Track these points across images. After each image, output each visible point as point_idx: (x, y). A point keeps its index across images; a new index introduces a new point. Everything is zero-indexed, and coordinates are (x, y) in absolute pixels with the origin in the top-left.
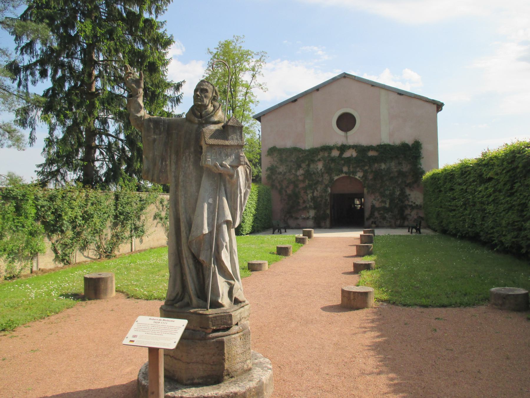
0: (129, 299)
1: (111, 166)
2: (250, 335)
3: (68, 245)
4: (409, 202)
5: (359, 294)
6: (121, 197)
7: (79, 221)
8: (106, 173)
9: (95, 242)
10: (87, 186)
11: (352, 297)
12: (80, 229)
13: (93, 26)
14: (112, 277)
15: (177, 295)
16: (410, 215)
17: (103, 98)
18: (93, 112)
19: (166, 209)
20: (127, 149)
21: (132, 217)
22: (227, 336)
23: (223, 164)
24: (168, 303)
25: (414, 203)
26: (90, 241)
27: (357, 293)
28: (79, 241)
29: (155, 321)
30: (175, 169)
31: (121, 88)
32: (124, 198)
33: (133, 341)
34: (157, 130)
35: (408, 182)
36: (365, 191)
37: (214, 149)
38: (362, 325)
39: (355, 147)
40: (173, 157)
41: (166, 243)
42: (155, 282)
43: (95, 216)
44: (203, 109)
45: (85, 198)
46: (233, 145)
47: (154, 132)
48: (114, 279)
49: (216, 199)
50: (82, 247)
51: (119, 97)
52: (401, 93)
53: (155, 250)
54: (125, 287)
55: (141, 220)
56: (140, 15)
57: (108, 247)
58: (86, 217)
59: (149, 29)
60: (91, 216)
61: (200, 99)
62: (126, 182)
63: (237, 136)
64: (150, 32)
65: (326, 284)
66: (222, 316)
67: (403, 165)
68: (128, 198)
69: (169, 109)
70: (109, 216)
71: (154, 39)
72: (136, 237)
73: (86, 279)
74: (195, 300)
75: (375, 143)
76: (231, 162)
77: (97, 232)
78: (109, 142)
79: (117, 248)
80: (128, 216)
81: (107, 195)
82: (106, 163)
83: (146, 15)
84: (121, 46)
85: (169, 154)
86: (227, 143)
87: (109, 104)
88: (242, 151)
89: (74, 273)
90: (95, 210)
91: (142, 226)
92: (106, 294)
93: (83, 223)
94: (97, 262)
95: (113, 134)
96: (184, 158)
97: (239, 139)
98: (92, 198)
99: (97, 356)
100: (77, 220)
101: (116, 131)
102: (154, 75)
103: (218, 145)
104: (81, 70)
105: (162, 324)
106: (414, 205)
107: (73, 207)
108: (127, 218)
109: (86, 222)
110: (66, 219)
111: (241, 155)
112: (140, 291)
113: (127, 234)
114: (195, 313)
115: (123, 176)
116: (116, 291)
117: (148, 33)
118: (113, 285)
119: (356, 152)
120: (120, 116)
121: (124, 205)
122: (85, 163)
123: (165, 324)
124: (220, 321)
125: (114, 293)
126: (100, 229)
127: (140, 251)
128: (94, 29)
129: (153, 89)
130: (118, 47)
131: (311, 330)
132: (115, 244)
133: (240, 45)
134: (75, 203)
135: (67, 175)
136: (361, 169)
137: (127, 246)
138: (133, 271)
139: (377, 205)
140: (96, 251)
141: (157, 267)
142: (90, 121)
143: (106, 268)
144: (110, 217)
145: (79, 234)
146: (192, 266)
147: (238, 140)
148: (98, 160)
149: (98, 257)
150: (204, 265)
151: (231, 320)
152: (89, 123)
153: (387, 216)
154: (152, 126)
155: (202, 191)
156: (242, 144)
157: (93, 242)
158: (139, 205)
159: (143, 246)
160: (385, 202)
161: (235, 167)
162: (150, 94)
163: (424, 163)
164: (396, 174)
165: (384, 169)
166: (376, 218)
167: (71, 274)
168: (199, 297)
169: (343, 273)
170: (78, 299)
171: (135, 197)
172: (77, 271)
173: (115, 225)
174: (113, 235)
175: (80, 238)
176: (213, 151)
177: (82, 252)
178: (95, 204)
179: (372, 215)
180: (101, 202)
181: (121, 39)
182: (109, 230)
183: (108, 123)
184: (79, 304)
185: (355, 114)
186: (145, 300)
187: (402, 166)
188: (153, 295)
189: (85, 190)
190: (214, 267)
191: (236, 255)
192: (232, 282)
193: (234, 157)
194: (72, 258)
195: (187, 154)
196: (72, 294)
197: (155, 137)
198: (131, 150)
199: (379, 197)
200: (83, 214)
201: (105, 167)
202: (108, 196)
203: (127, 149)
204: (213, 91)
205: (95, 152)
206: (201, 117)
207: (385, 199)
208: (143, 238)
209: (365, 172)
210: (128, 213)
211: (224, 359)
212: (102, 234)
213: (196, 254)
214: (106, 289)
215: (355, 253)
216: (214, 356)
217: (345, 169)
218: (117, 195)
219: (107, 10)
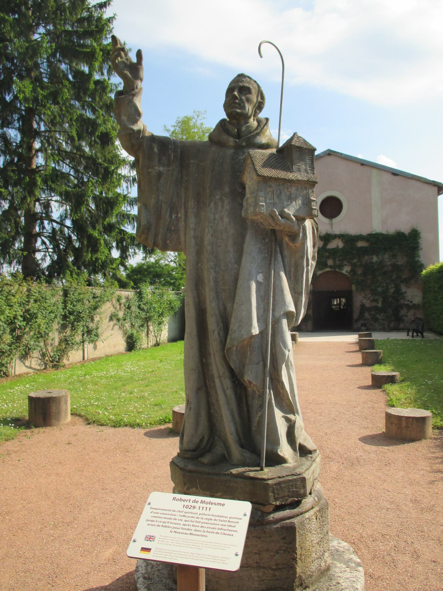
0: (89, 426)
1: (56, 257)
2: (327, 509)
3: (6, 352)
4: (405, 300)
5: (414, 421)
6: (71, 293)
7: (20, 322)
8: (49, 266)
9: (39, 349)
10: (29, 278)
11: (404, 424)
12: (20, 332)
13: (33, 87)
14: (66, 396)
15: (202, 440)
16: (407, 316)
17: (46, 175)
18: (34, 191)
19: (124, 308)
20: (74, 237)
21: (84, 317)
22: (298, 515)
23: (285, 211)
24: (187, 455)
25: (411, 302)
26: (33, 348)
27: (411, 419)
28: (19, 347)
29: (186, 503)
30: (195, 225)
31: (67, 164)
32: (75, 294)
33: (148, 550)
34: (164, 158)
35: (403, 277)
36: (354, 287)
37: (270, 186)
38: (435, 467)
39: (342, 237)
40: (191, 203)
41: (124, 350)
42: (121, 402)
43: (39, 316)
44: (243, 122)
45: (27, 293)
46: (301, 181)
47: (159, 161)
48: (69, 399)
49: (270, 274)
50: (22, 354)
51: (65, 176)
52: (395, 173)
53: (113, 358)
54: (82, 408)
55: (95, 321)
56: (90, 75)
57: (55, 355)
58: (28, 318)
59: (100, 93)
60: (34, 316)
61: (240, 104)
62: (75, 276)
63: (306, 166)
64: (102, 96)
65: (345, 403)
66: (290, 481)
67: (399, 257)
68: (79, 294)
69: (123, 190)
70: (56, 317)
71: (107, 104)
72: (89, 343)
73: (31, 399)
74: (236, 451)
75: (365, 232)
76: (297, 211)
77: (41, 336)
78: (54, 229)
79: (66, 355)
80: (79, 316)
81: (54, 290)
82: (49, 255)
83: (97, 77)
84: (68, 112)
85: (183, 201)
86: (291, 176)
87: (53, 182)
88: (313, 192)
89: (14, 388)
90: (39, 308)
91: (96, 329)
92: (58, 419)
93: (25, 325)
94: (42, 374)
95: (58, 220)
96: (212, 205)
97: (309, 171)
98: (35, 293)
99: (55, 526)
100: (16, 321)
101: (61, 216)
102: (107, 149)
103: (277, 179)
104: (18, 142)
105: (201, 511)
106: (410, 304)
107: (12, 304)
108: (78, 319)
109: (27, 324)
110: (3, 320)
111: (312, 198)
112: (102, 414)
113: (78, 338)
114: (241, 476)
115: (70, 269)
116: (72, 414)
117: (100, 98)
118: (68, 407)
119: (343, 243)
120: (66, 197)
121: (75, 303)
122: (25, 253)
123: (207, 512)
124: (287, 490)
125: (69, 418)
126: (45, 332)
127: (94, 360)
128: (34, 90)
129: (106, 165)
130: (63, 113)
131: (365, 475)
132: (63, 351)
133: (201, 122)
134: (14, 300)
135: (3, 268)
136: (349, 262)
137: (78, 353)
138: (90, 386)
139: (368, 304)
140: (40, 359)
141: (121, 381)
142: (31, 201)
143: (54, 382)
144: (58, 317)
145: (18, 338)
146: (230, 392)
147: (307, 173)
148: (39, 251)
149: (43, 367)
150: (250, 390)
151: (304, 487)
152: (29, 205)
153: (379, 317)
154: (156, 150)
155: (246, 260)
156: (314, 180)
157: (37, 349)
158: (93, 302)
159: (98, 353)
160: (377, 301)
161: (301, 220)
162: (103, 170)
163: (423, 256)
164: (390, 268)
165: (376, 261)
166: (366, 320)
167: (9, 390)
168: (242, 446)
169: (359, 388)
170: (20, 426)
171: (87, 293)
172: (17, 386)
173: (64, 327)
174: (61, 340)
175: (20, 343)
176: (269, 189)
177: (22, 362)
178: (39, 300)
179: (362, 313)
180: (46, 299)
181: (67, 104)
182: (57, 334)
183: (51, 207)
184: (23, 434)
185: (342, 198)
186: (112, 426)
187: (397, 258)
188: (122, 420)
189: (26, 283)
190: (270, 394)
191: (293, 371)
192: (291, 416)
193: (300, 202)
194: (11, 369)
195: (218, 197)
196: (12, 419)
197: (161, 169)
198: (79, 240)
199: (370, 296)
200: (24, 313)
201: (48, 259)
202: (55, 291)
203: (74, 237)
204: (258, 93)
205: (36, 241)
206: (238, 136)
207: (376, 297)
208: (97, 343)
209: (354, 266)
210: (79, 312)
211: (295, 559)
212: (47, 339)
213: (237, 371)
214: (59, 413)
215: (360, 361)
216: (277, 553)
217: (330, 262)
218: (66, 290)
219: (49, 70)
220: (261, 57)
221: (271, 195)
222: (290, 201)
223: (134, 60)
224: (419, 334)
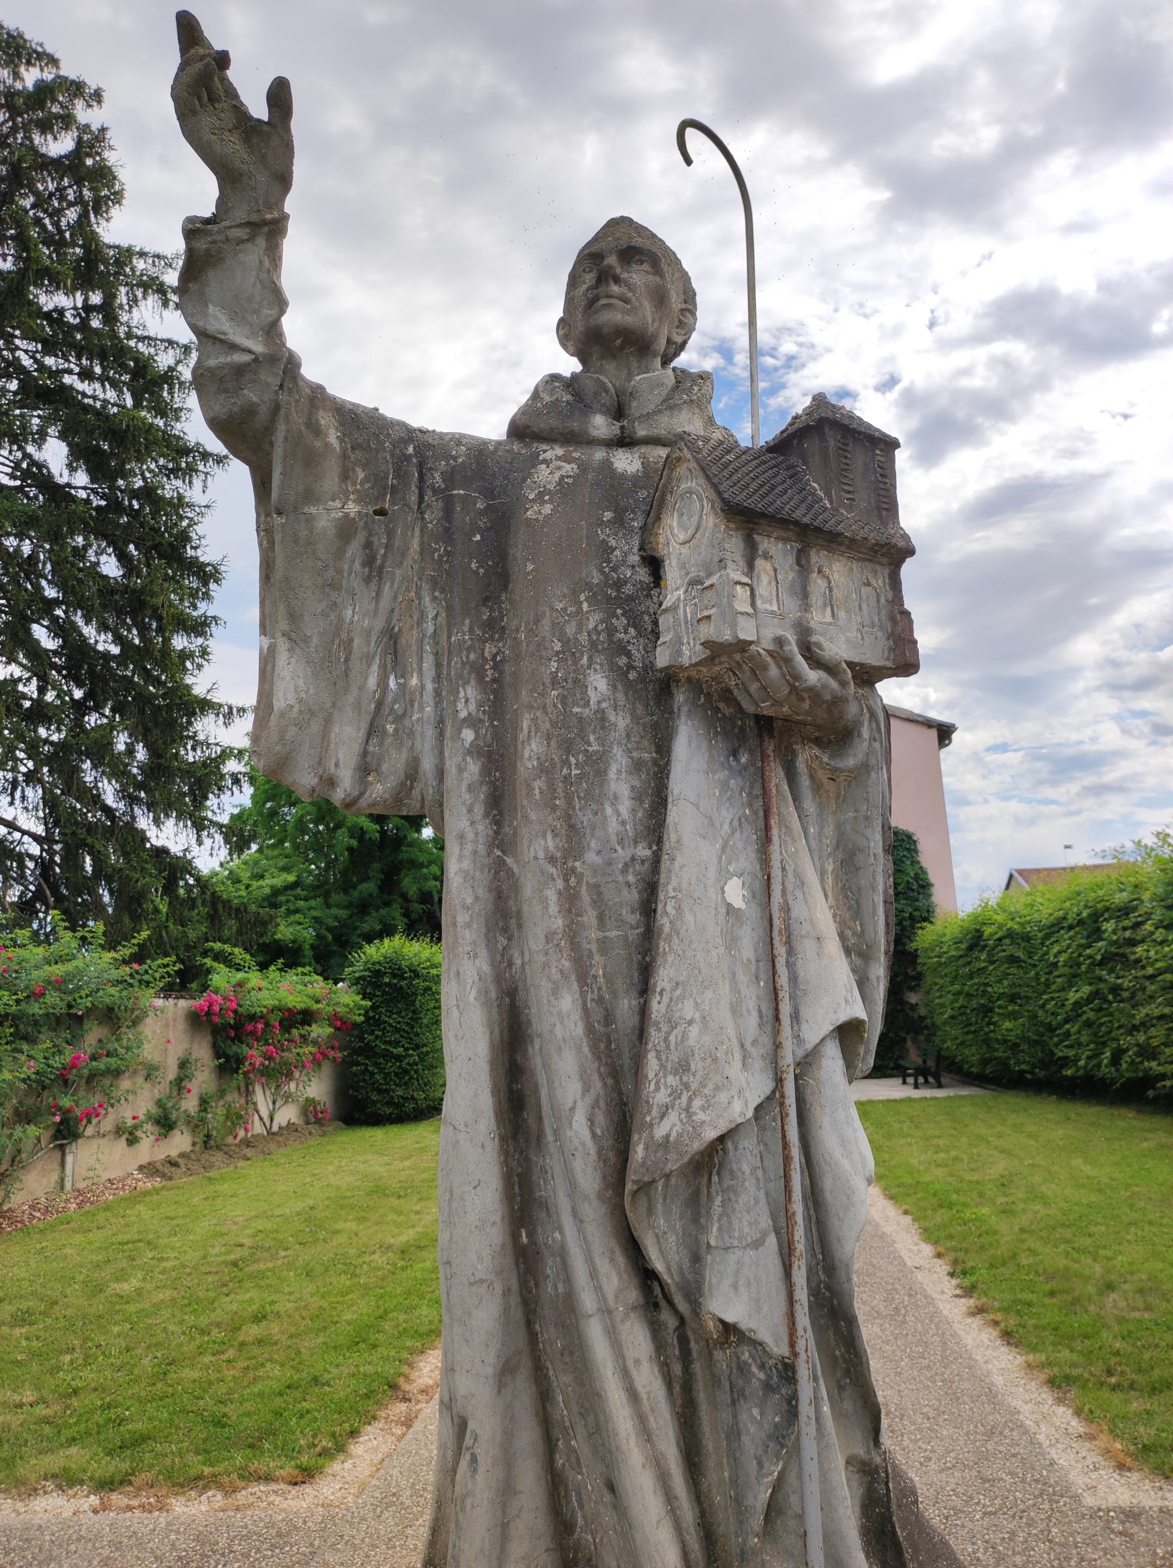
220: (688, 161)
221: (770, 583)
222: (829, 609)
223: (259, 109)
224: (931, 1079)
